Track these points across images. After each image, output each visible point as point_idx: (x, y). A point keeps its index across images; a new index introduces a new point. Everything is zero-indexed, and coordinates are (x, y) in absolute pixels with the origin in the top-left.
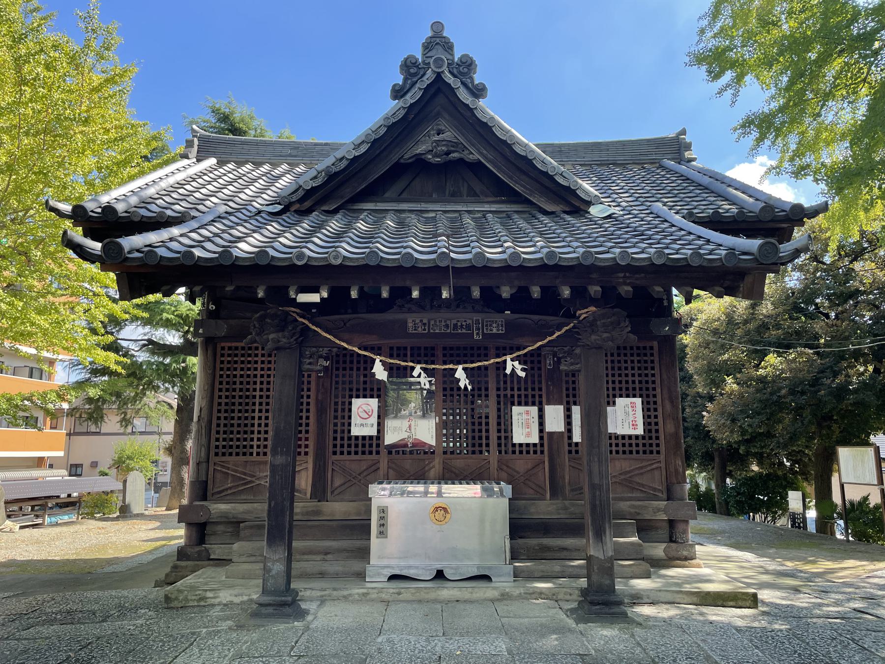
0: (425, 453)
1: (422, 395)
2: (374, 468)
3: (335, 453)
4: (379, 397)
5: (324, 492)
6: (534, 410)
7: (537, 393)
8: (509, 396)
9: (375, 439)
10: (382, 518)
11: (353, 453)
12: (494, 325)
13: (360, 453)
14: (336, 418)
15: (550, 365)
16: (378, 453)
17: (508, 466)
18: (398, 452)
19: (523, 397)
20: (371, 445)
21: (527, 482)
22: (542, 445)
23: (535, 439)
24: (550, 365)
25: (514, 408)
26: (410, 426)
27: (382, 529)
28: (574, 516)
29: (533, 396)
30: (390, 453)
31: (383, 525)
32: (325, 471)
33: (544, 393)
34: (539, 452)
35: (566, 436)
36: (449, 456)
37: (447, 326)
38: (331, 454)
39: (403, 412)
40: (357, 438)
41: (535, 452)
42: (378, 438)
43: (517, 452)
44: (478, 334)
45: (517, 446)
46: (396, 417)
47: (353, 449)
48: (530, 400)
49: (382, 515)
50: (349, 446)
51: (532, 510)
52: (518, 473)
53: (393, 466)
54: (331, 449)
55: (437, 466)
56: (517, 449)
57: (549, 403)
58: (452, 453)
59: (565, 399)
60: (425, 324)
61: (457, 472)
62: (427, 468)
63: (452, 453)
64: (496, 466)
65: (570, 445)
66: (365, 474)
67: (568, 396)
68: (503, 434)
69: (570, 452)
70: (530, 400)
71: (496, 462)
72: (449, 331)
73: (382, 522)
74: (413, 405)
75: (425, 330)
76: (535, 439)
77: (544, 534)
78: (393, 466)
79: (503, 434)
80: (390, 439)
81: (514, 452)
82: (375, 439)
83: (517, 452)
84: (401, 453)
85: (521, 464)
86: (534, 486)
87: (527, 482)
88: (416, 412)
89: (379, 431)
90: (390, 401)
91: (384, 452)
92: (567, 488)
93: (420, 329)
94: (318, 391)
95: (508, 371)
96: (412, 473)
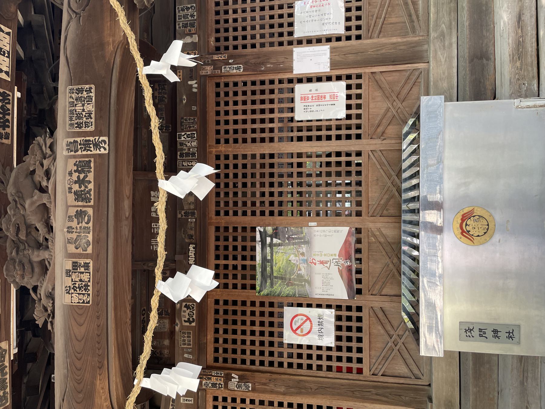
0: (359, 241)
1: (279, 245)
2: (380, 315)
3: (360, 371)
4: (281, 306)
5: (416, 390)
6: (300, 89)
7: (276, 86)
8: (280, 125)
9: (339, 313)
10: (482, 333)
11: (360, 345)
12: (79, 108)
13: (359, 335)
14: (310, 367)
15: (239, 68)
16: (359, 309)
17: (379, 126)
18: (359, 281)
19: (282, 105)
20: (349, 319)
21: (402, 96)
22: (349, 77)
23: (339, 88)
24: (239, 68)
25: (297, 118)
26: (322, 262)
27: (503, 335)
28: (454, 23)
29: (281, 91)
30: (359, 291)
31: (495, 331)
32: (385, 387)
33: (276, 77)
34: (359, 81)
35: (335, 44)
36: (363, 209)
37: (80, 215)
38: (360, 377)
39: (303, 272)
40: (338, 338)
41: (359, 86)
42: (339, 308)
43: (359, 111)
44: (97, 145)
45: (350, 112)
46: (309, 282)
47: (354, 334)
48: (286, 95)
49: (476, 333)
50: (349, 360)
51: (445, 85)
52: (388, 110)
53: (377, 287)
54: (354, 376)
55: (379, 225)
56: (354, 112)
57: (291, 70)
58: (359, 204)
59: (286, 47)
60: (75, 266)
61: (386, 196)
62: (382, 240)
63: (359, 204)
64: (378, 141)
65: (348, 38)
66: (389, 328)
67: (281, 44)
68: (333, 133)
69: (358, 37)
70: (286, 95)
71: (373, 142)
72: (90, 211)
73: (489, 334)
74: (292, 257)
75: (86, 266)
76: (339, 88)
77: (488, 59)
78: (377, 287)
79: (333, 133)
80: (339, 292)
81: (359, 116)
82: (339, 313)
83: (359, 111)
84: (359, 276)
85: (375, 106)
86: (407, 87)
87: (402, 96)
88: (303, 254)
89: (329, 307)
90: (287, 290)
91: (357, 301)
92: (411, 39)
93: (85, 277)
94: (272, 392)
95: (173, 78)
96: (388, 260)
